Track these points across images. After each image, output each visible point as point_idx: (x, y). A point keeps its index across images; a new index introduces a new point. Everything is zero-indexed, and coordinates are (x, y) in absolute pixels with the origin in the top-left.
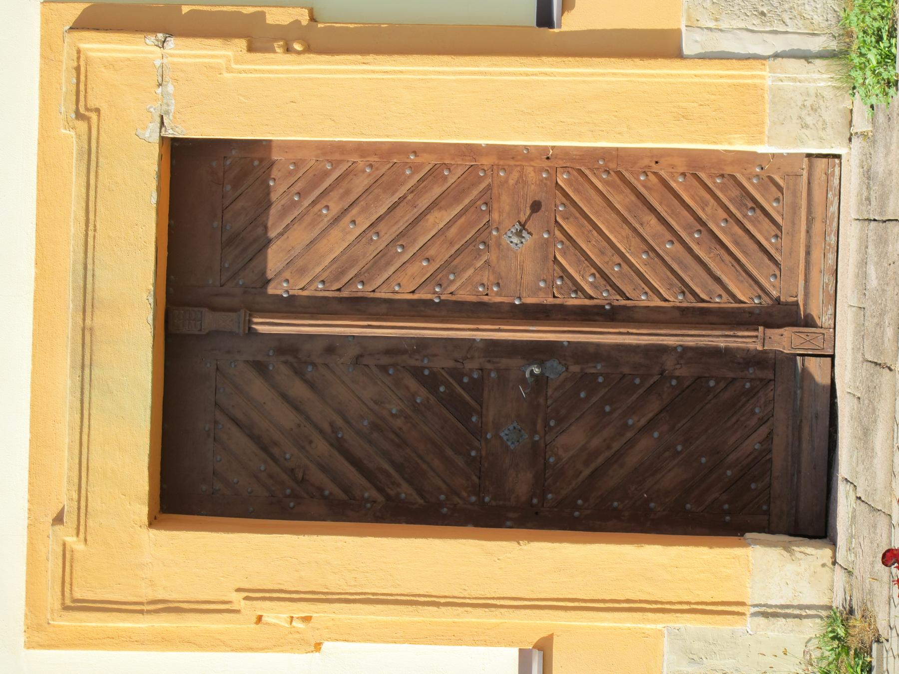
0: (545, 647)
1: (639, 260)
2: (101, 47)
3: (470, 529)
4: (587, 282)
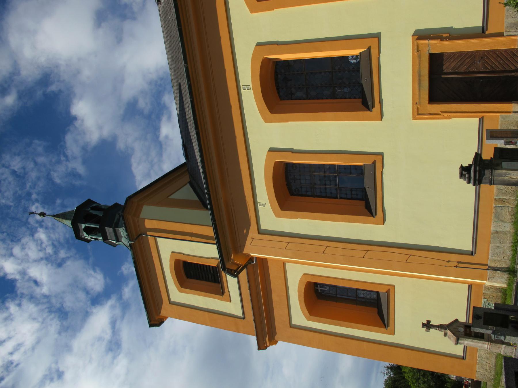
0: (482, 118)
1: (497, 64)
2: (420, 42)
3: (203, 293)
4: (489, 68)
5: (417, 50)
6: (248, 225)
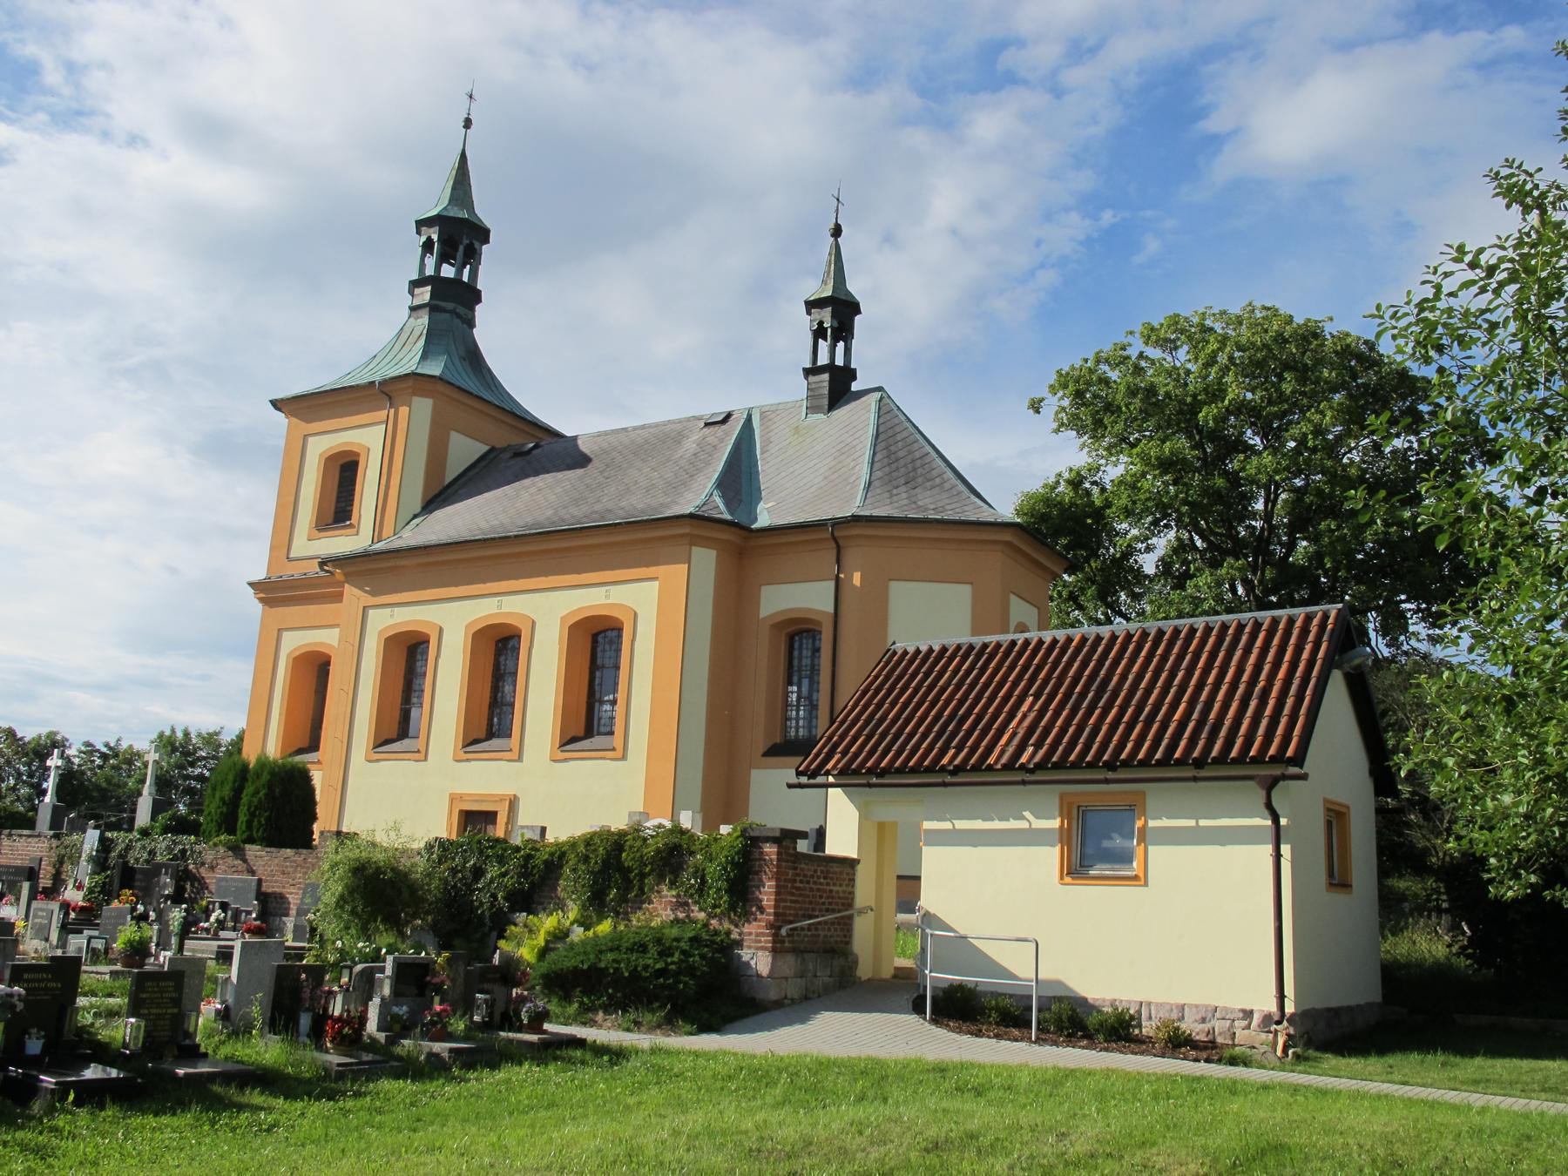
5: (501, 799)
6: (373, 593)
